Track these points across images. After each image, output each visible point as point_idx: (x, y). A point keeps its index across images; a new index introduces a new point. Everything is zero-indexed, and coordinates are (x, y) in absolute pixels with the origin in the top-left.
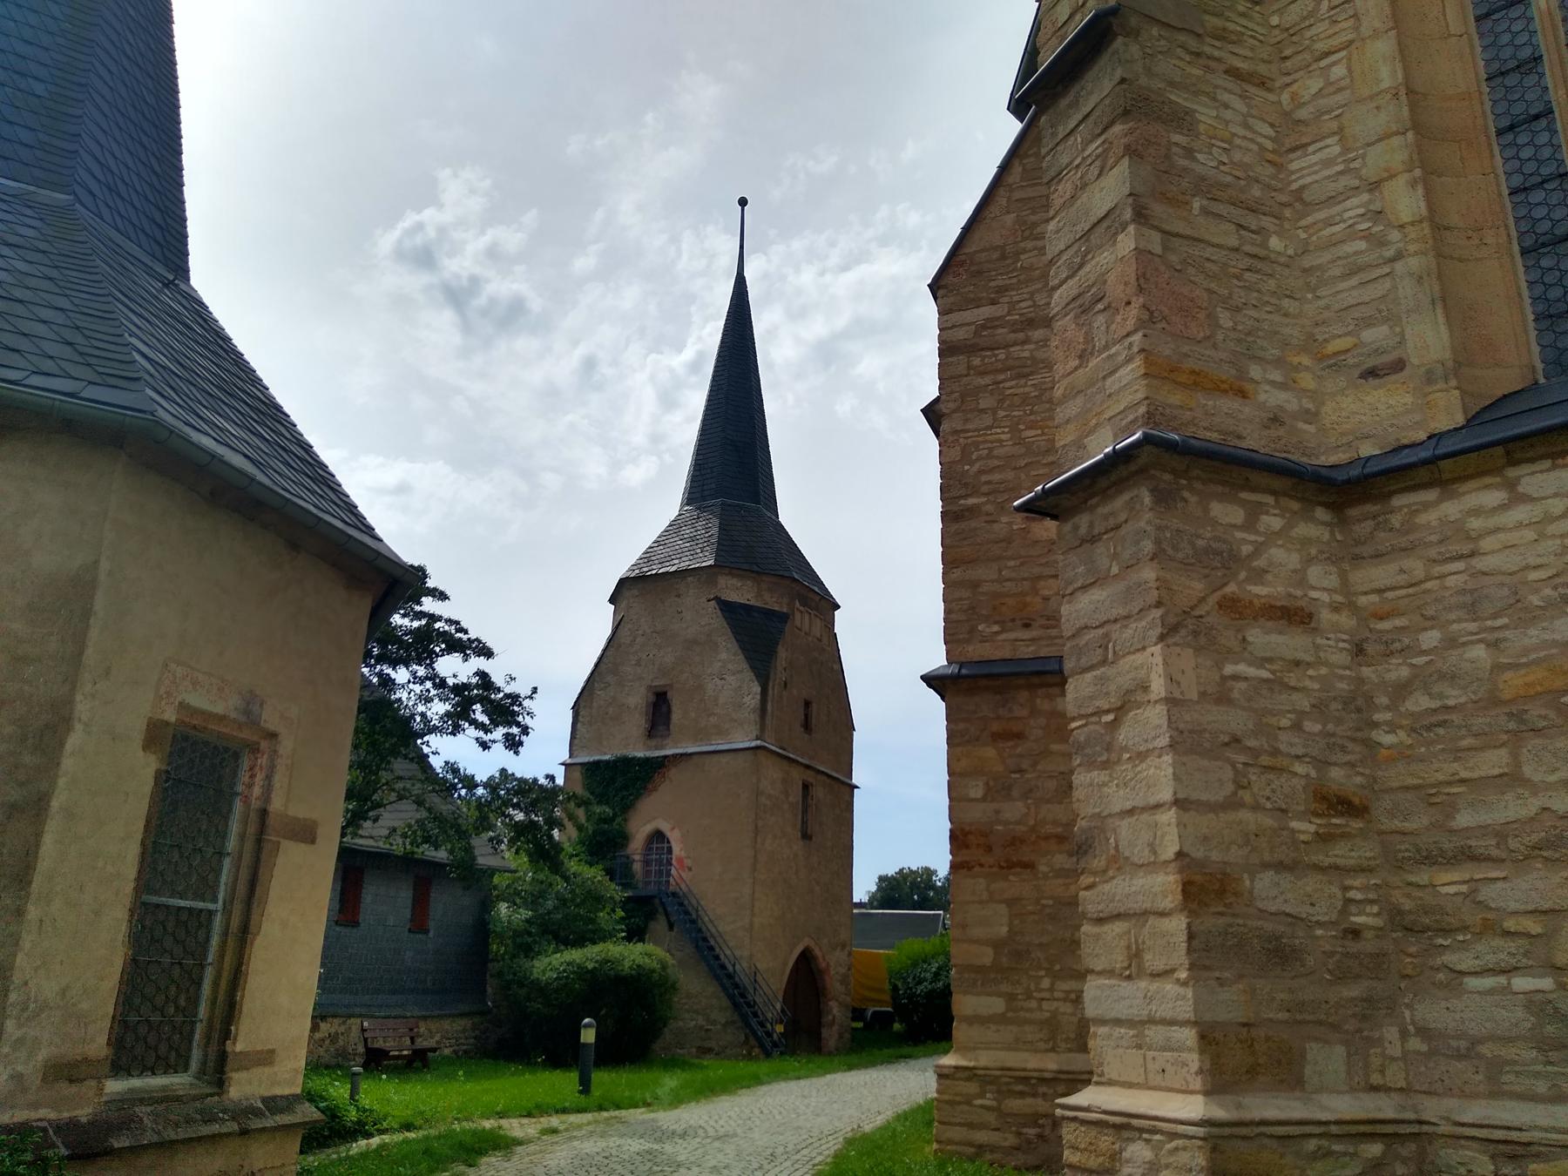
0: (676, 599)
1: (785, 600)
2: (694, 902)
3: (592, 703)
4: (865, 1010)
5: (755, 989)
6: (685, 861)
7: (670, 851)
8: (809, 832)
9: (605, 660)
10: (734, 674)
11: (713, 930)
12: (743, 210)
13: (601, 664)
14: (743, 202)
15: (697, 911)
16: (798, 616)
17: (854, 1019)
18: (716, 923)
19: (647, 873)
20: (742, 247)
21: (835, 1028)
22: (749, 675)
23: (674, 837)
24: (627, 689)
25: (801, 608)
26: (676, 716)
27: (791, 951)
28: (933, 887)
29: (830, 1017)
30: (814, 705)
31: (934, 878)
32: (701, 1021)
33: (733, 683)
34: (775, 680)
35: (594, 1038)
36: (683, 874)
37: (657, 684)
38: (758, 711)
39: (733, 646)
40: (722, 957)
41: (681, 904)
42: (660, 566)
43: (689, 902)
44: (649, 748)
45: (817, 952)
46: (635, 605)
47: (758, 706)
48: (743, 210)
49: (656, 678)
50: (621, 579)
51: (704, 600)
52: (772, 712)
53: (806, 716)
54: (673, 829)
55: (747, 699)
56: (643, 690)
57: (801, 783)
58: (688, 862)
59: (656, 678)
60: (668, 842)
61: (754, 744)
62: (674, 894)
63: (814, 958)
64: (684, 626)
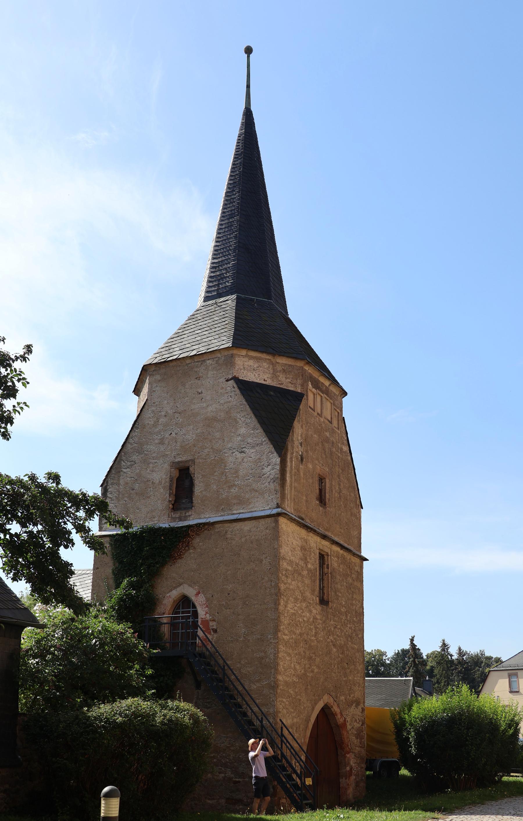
0: (197, 381)
1: (299, 381)
2: (221, 662)
3: (119, 480)
4: (374, 760)
5: (282, 741)
6: (211, 624)
7: (195, 614)
8: (325, 597)
9: (131, 441)
10: (253, 447)
11: (240, 688)
12: (248, 57)
13: (127, 444)
14: (249, 51)
15: (223, 669)
16: (311, 396)
17: (367, 769)
18: (242, 681)
19: (174, 635)
20: (248, 86)
21: (353, 777)
22: (268, 447)
23: (199, 601)
24: (151, 465)
25: (314, 390)
26: (199, 489)
27: (313, 709)
28: (383, 664)
29: (348, 768)
30: (327, 481)
31: (384, 658)
32: (229, 774)
33: (252, 456)
34: (292, 453)
35: (118, 812)
36: (209, 636)
37: (180, 460)
38: (278, 481)
39: (253, 421)
40: (249, 713)
41: (208, 664)
42: (180, 352)
43: (216, 661)
44: (174, 519)
45: (336, 709)
46: (158, 388)
47: (278, 476)
48: (248, 57)
49: (178, 455)
50: (144, 366)
51: (223, 380)
52: (291, 485)
53: (320, 490)
54: (198, 594)
55: (267, 470)
56: (166, 466)
57: (317, 552)
58: (213, 625)
59: (178, 455)
60: (194, 606)
61: (275, 511)
62: (201, 655)
63: (334, 715)
64: (205, 405)
